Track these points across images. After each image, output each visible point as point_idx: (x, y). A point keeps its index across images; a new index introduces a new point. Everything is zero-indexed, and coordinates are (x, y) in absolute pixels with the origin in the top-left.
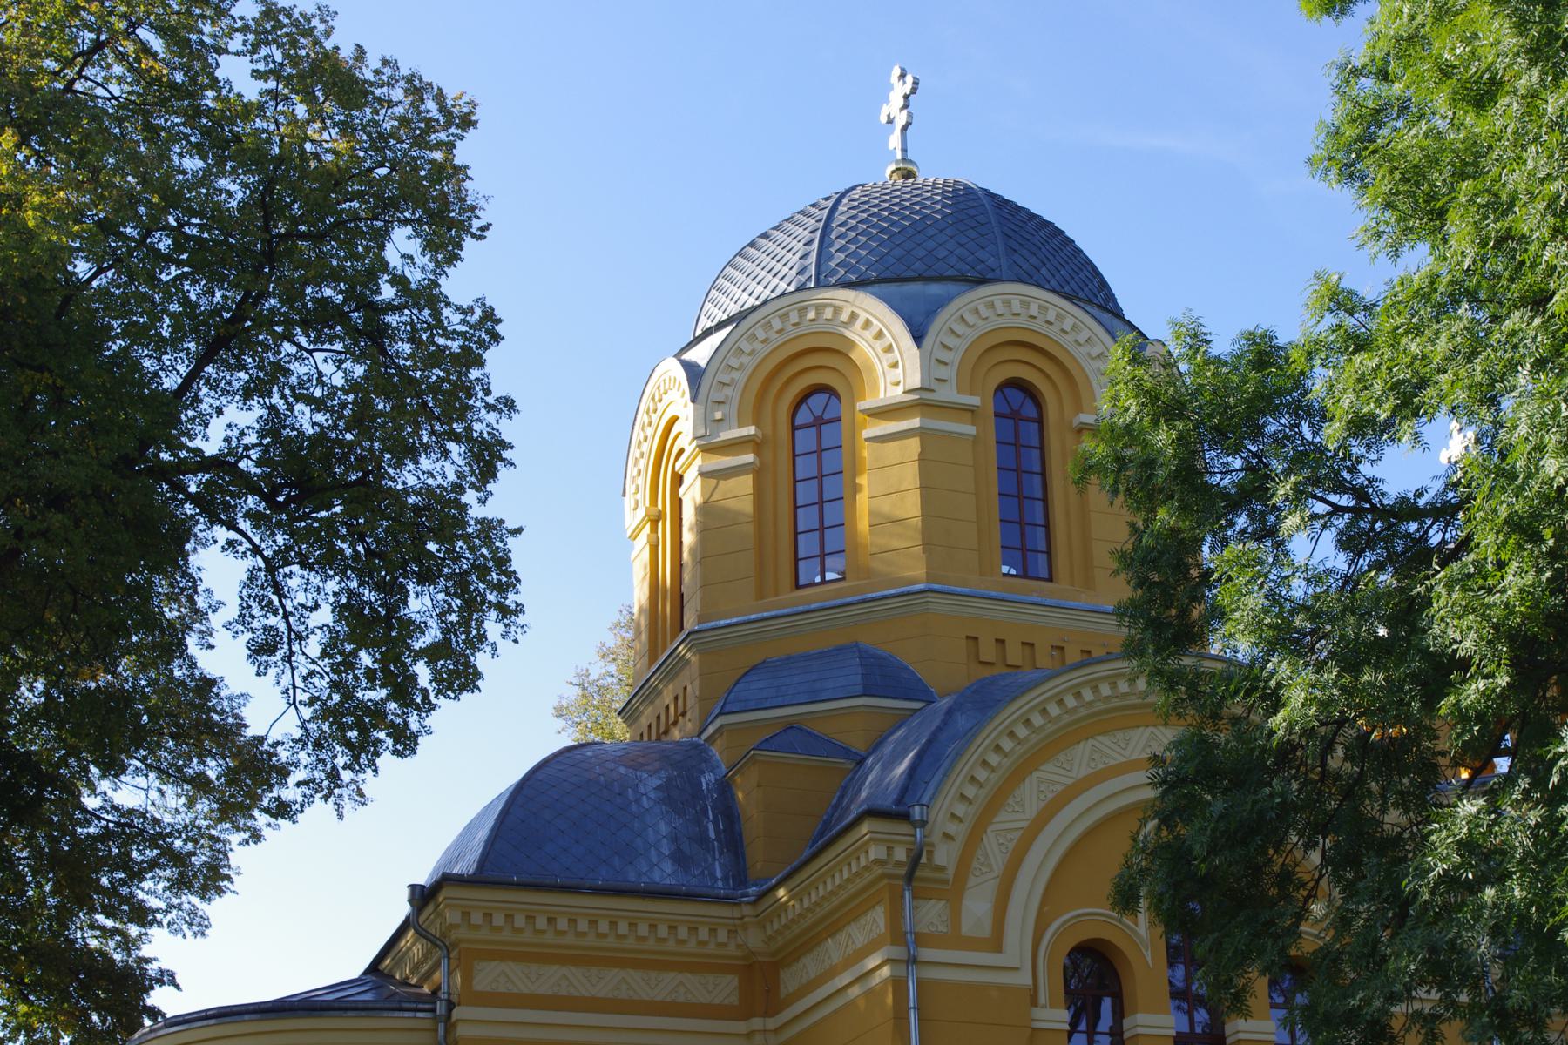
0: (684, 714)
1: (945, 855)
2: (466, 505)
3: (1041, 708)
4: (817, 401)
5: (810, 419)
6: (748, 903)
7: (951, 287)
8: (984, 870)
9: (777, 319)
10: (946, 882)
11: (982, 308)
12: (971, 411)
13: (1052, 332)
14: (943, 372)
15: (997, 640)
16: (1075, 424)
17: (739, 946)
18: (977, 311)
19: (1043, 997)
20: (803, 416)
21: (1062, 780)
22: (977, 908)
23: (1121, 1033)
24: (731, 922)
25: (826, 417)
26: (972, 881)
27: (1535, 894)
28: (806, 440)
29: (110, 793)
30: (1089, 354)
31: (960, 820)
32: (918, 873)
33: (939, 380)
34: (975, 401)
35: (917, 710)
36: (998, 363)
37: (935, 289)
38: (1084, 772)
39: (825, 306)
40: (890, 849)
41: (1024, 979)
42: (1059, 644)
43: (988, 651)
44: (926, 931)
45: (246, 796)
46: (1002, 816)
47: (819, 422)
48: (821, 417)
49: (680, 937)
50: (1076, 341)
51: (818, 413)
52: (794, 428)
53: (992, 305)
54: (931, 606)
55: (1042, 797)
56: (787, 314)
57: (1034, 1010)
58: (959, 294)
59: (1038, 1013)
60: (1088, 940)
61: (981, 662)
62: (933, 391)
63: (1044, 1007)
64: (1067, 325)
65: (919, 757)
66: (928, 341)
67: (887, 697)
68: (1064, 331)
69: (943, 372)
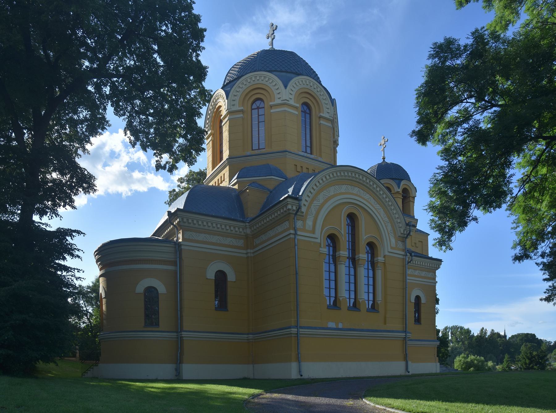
0: (224, 180)
1: (304, 209)
2: (200, 113)
3: (321, 178)
4: (258, 103)
5: (256, 107)
6: (247, 222)
7: (292, 75)
8: (311, 214)
9: (249, 79)
10: (303, 216)
11: (300, 81)
12: (296, 108)
13: (315, 91)
14: (291, 96)
15: (301, 166)
16: (319, 116)
17: (244, 233)
18: (299, 82)
19: (322, 246)
20: (254, 106)
21: (328, 195)
22: (309, 223)
23: (335, 256)
24: (243, 227)
25: (260, 107)
26: (308, 217)
27: (509, 188)
28: (255, 112)
29: (73, 196)
30: (323, 98)
31: (307, 201)
32: (298, 213)
33: (290, 98)
34: (298, 105)
35: (284, 181)
36: (303, 97)
37: (289, 75)
38: (333, 194)
39: (261, 76)
40: (292, 206)
41: (318, 241)
42: (314, 169)
43: (299, 169)
44: (298, 227)
45: (445, 50)
46: (315, 202)
47: (258, 108)
48: (259, 107)
49: (231, 229)
50: (320, 94)
51: (258, 106)
52: (252, 109)
53: (302, 81)
54: (287, 156)
55: (334, 192)
56: (256, 77)
57: (320, 248)
58: (295, 77)
59: (321, 249)
60: (330, 234)
61: (298, 171)
62: (289, 101)
63: (322, 248)
64: (319, 90)
65: (311, 180)
66: (288, 88)
67: (279, 177)
68: (318, 91)
69: (291, 96)
